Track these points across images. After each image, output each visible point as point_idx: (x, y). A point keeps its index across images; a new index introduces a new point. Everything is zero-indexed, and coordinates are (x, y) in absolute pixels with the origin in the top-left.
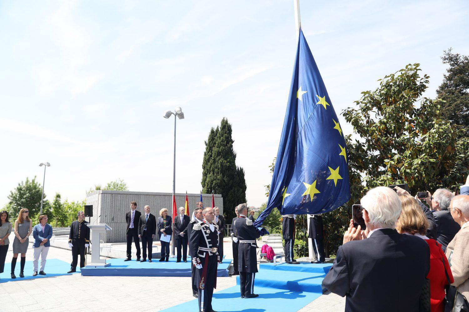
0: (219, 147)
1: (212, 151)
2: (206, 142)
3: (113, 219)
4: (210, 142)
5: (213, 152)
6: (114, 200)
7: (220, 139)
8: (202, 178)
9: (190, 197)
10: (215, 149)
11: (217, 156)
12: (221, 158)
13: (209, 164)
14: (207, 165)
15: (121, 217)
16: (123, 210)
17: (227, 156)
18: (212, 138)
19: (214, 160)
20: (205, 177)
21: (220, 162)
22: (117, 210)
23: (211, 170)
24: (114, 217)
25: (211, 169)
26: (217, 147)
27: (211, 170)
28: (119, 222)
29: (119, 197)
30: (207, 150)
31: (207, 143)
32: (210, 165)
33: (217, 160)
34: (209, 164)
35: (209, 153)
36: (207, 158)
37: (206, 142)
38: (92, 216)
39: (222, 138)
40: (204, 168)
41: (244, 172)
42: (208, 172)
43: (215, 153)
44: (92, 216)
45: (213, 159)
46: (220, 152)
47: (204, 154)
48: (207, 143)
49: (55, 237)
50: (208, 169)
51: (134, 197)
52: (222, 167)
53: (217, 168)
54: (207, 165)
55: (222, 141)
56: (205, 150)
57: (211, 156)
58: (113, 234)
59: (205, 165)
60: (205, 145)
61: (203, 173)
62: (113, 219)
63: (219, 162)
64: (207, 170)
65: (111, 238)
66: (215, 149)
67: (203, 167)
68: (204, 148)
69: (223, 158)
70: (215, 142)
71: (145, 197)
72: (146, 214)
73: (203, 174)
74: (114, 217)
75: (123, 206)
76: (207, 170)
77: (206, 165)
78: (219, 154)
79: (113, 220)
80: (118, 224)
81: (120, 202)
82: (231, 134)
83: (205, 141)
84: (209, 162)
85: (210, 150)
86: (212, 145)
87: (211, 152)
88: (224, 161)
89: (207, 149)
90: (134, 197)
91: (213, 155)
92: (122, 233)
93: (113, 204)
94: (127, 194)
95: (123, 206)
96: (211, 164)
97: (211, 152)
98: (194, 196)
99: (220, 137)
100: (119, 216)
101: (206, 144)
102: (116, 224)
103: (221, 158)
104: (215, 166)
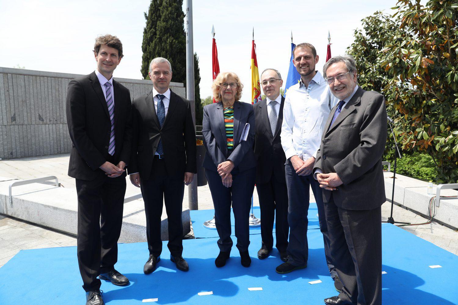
0: (167, 22)
1: (156, 26)
2: (146, 14)
3: (14, 119)
4: (152, 14)
5: (157, 28)
6: (10, 84)
7: (167, 10)
8: (142, 64)
9: (141, 85)
10: (161, 24)
11: (164, 35)
12: (170, 36)
13: (152, 45)
14: (149, 46)
15: (29, 115)
16: (32, 103)
17: (177, 35)
18: (155, 8)
19: (160, 39)
20: (146, 63)
21: (169, 42)
22: (21, 103)
23: (156, 53)
24: (15, 114)
25: (156, 52)
26: (163, 21)
27: (156, 53)
28: (26, 123)
29: (21, 79)
30: (149, 25)
31: (147, 15)
32: (153, 46)
33: (164, 39)
34: (152, 45)
35: (152, 29)
36: (149, 36)
37: (146, 14)
38: (213, 39)
39: (170, 9)
40: (144, 50)
41: (197, 58)
42: (150, 56)
43: (161, 30)
44: (213, 39)
45: (158, 38)
46: (168, 29)
47: (143, 31)
48: (147, 15)
49: (442, 188)
50: (151, 52)
51: (49, 81)
52: (172, 49)
53: (164, 50)
54: (149, 46)
55: (171, 13)
56: (145, 25)
57: (155, 34)
58: (17, 143)
59: (147, 46)
60: (145, 18)
61: (143, 57)
62: (14, 119)
63: (168, 42)
64: (150, 53)
65: (14, 151)
66: (161, 24)
67: (143, 49)
68: (143, 23)
69: (173, 37)
70: (159, 14)
71: (46, 80)
72: (155, 93)
73: (143, 59)
74: (15, 114)
75: (32, 96)
76: (150, 53)
77: (148, 47)
78: (166, 30)
79: (15, 120)
80: (24, 126)
81: (23, 89)
82: (182, 5)
83: (145, 12)
84: (152, 42)
85: (152, 25)
86: (156, 18)
87: (155, 29)
88: (174, 40)
89: (148, 24)
90: (49, 81)
91: (158, 33)
92: (33, 141)
93: (11, 91)
94: (36, 76)
95: (32, 96)
96: (156, 45)
97: (155, 29)
98: (147, 84)
99: (167, 7)
100: (25, 114)
101: (147, 18)
102: (28, 126)
103: (170, 36)
104: (161, 48)
